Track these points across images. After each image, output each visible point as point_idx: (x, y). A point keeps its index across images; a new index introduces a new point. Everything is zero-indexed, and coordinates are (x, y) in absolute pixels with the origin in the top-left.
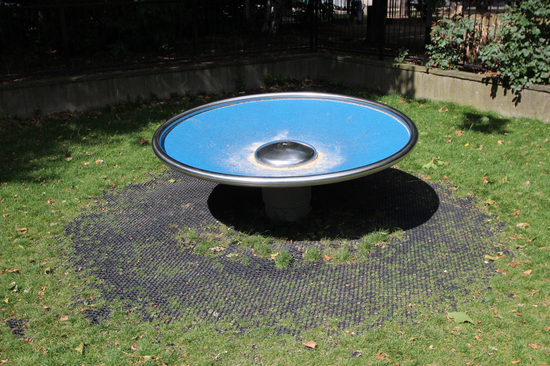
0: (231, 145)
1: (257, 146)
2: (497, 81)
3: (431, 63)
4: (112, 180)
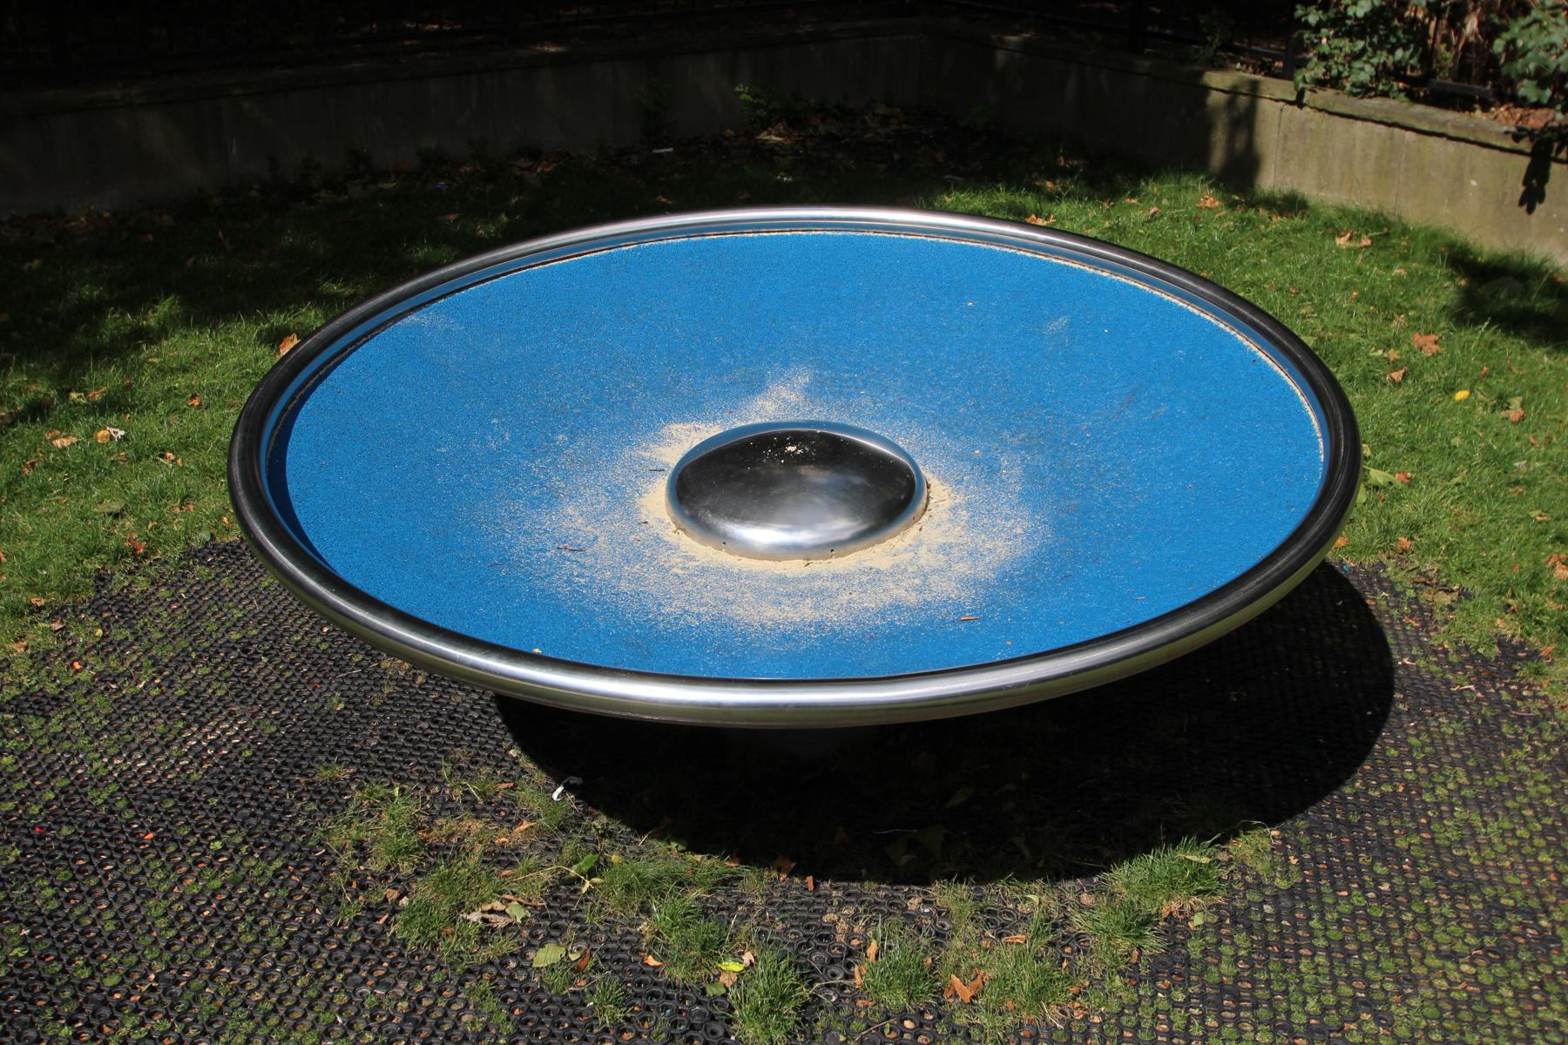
0: (573, 435)
1: (683, 439)
2: (1549, 143)
3: (1316, 70)
4: (142, 522)
